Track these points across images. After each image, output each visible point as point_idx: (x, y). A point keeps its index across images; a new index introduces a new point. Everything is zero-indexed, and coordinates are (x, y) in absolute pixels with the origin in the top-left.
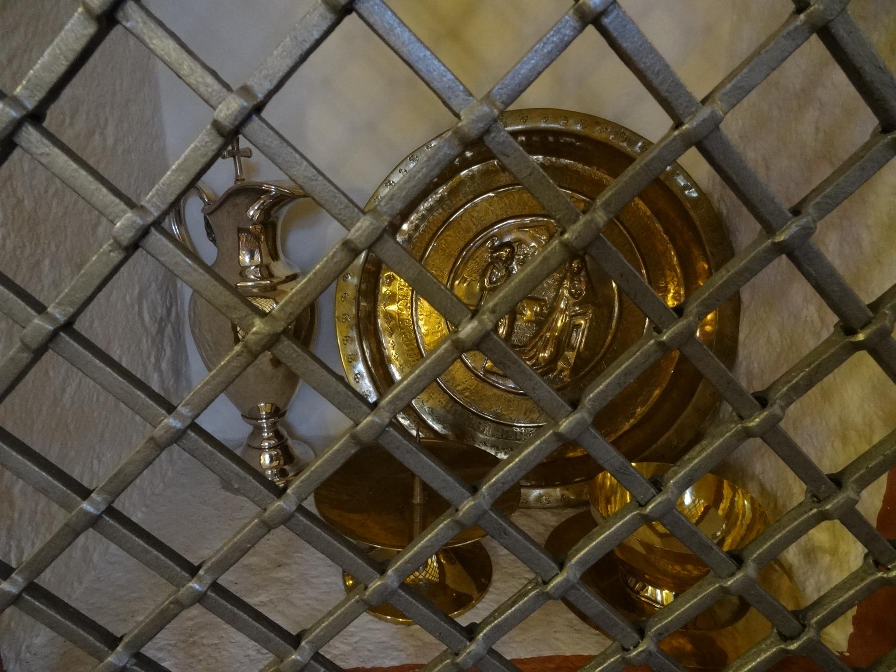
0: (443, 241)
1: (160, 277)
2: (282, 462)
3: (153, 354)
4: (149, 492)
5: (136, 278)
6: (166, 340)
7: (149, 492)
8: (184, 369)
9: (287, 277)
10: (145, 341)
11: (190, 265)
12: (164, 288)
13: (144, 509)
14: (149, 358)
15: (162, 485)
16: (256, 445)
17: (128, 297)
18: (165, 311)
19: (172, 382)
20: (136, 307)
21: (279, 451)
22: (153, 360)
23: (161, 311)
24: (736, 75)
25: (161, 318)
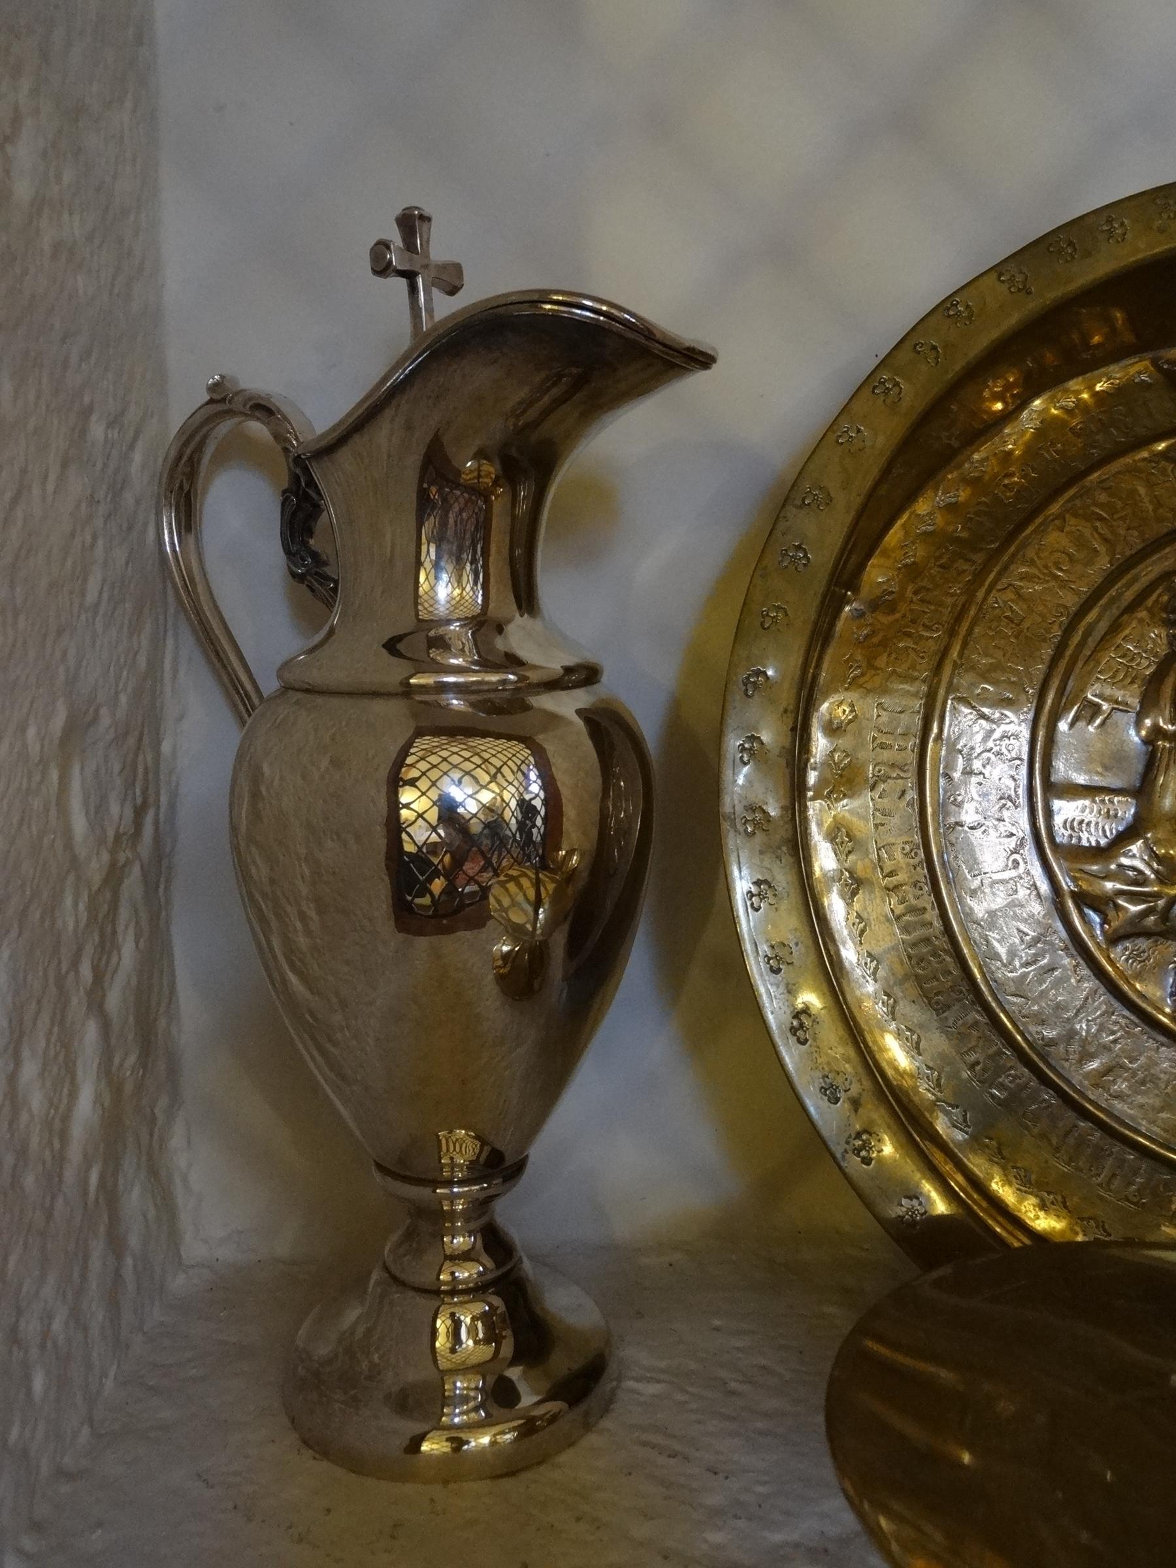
0: (1010, 595)
1: (123, 699)
2: (507, 1349)
3: (89, 949)
4: (45, 1469)
5: (62, 677)
6: (124, 913)
7: (45, 1469)
8: (162, 1022)
9: (568, 670)
10: (68, 901)
11: (333, 505)
12: (131, 741)
13: (28, 1543)
14: (75, 964)
15: (86, 1431)
16: (424, 1278)
17: (32, 732)
18: (129, 813)
19: (132, 1059)
20: (54, 775)
21: (497, 1301)
22: (86, 971)
23: (118, 812)
24: (1100, 598)
25: (118, 837)
